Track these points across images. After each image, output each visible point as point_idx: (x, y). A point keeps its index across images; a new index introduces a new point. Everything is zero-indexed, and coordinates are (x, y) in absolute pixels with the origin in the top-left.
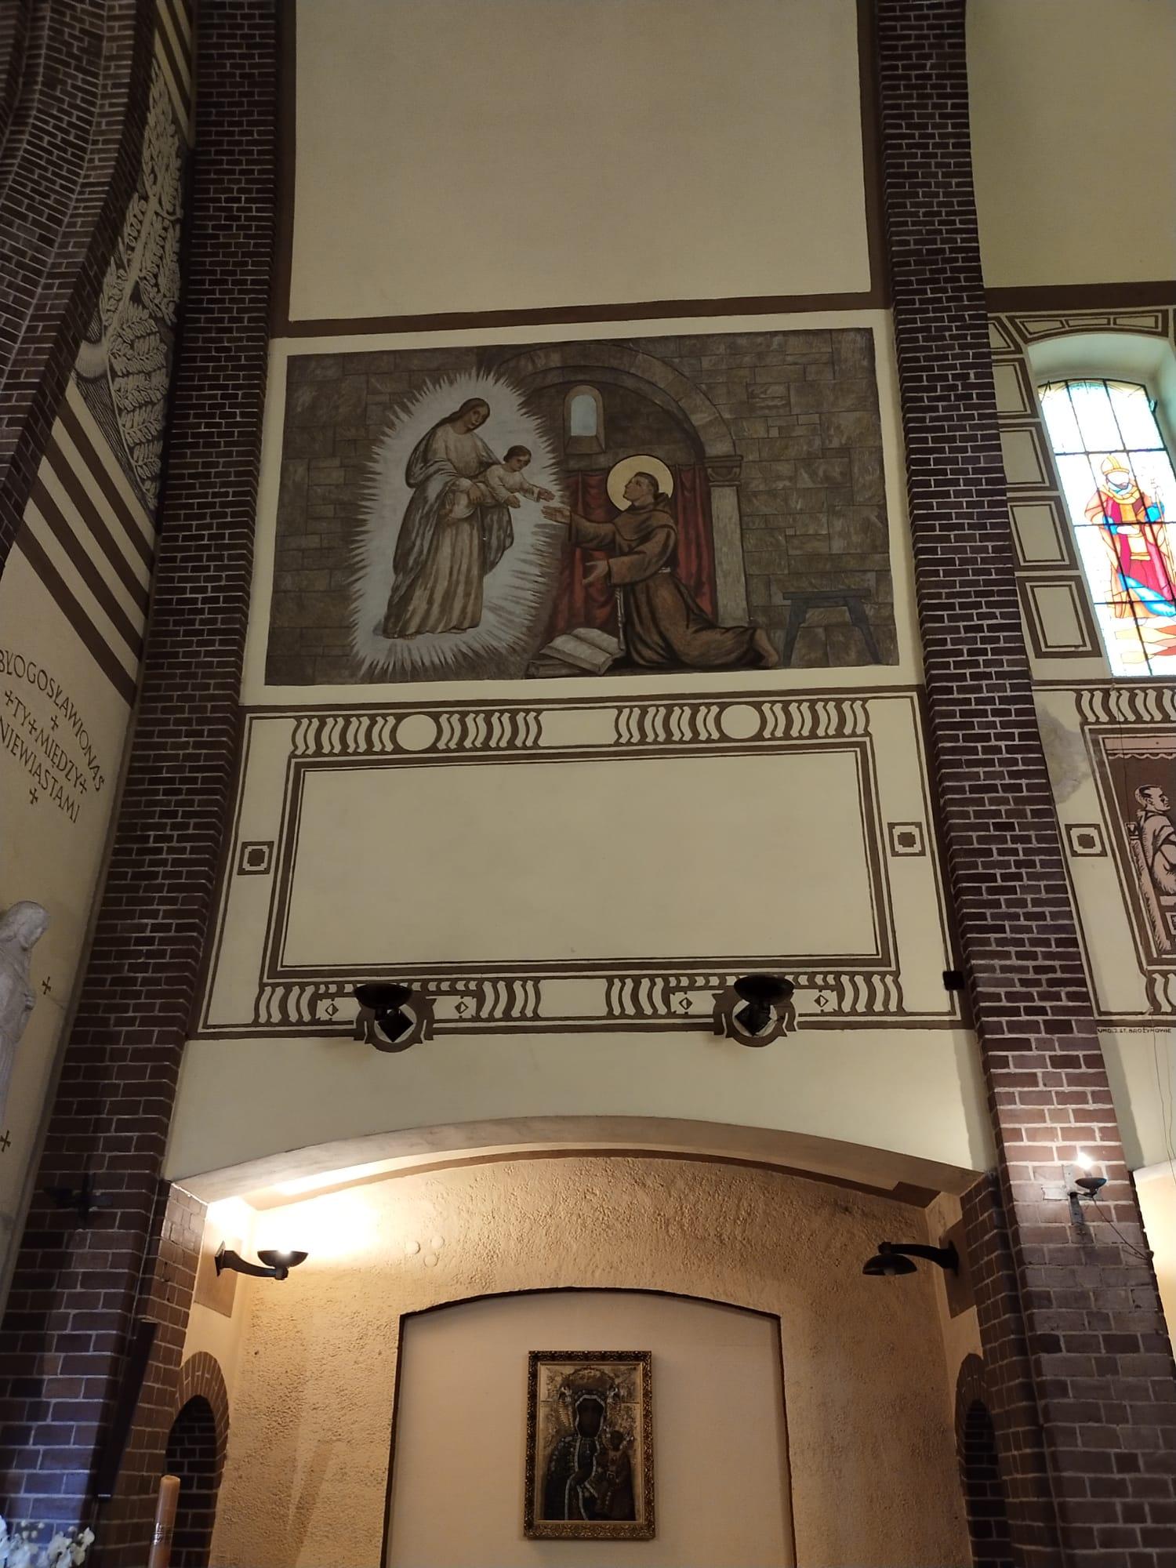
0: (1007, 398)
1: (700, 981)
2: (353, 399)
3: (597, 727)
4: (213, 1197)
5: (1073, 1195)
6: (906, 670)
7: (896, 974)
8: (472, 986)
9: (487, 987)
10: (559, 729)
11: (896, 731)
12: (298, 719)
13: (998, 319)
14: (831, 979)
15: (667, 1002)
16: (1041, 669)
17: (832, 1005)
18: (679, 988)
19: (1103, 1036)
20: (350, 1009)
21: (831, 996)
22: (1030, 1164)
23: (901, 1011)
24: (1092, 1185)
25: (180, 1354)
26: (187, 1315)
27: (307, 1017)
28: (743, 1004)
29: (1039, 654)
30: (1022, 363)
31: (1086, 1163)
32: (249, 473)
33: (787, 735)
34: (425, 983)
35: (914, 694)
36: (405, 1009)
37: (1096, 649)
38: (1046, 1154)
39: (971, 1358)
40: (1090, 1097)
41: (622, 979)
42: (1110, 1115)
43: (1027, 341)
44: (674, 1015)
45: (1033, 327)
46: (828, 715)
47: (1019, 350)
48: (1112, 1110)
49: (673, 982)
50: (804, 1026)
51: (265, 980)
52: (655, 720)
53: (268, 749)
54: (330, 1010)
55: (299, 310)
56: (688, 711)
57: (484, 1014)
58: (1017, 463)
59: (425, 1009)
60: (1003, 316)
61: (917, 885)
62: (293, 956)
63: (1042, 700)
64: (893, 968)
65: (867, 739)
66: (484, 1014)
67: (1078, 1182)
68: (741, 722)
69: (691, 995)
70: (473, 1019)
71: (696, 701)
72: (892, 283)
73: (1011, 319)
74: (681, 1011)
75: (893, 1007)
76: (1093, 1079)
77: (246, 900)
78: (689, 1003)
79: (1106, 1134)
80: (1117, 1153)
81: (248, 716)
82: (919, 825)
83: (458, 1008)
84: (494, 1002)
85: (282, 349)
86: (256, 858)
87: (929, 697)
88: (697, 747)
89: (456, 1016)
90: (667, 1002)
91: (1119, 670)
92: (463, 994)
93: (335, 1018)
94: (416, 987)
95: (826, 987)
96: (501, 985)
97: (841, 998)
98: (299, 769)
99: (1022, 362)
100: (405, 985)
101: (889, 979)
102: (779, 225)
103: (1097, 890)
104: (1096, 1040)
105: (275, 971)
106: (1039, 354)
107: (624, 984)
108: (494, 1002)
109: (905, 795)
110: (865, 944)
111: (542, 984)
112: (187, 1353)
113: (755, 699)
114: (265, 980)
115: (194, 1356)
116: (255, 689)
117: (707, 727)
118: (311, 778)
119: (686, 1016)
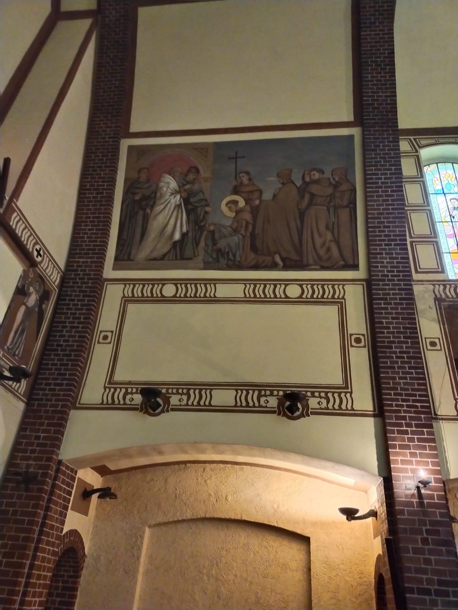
0: (408, 167)
1: (317, 394)
2: (151, 163)
3: (237, 291)
4: (103, 480)
5: (418, 488)
6: (361, 273)
7: (351, 393)
8: (185, 391)
9: (191, 392)
10: (223, 291)
11: (355, 298)
12: (125, 285)
13: (410, 139)
14: (323, 395)
15: (259, 401)
16: (415, 276)
17: (324, 405)
18: (265, 396)
19: (434, 424)
20: (138, 398)
21: (324, 401)
22: (401, 475)
23: (353, 409)
24: (425, 484)
25: (62, 529)
26: (66, 514)
27: (257, 404)
28: (288, 403)
29: (417, 272)
30: (418, 157)
31: (423, 474)
32: (112, 189)
33: (312, 297)
34: (168, 389)
35: (364, 283)
36: (159, 400)
37: (443, 272)
38: (406, 471)
39: (379, 555)
40: (416, 440)
41: (242, 390)
42: (436, 456)
43: (420, 147)
44: (262, 407)
45: (423, 142)
46: (329, 290)
47: (417, 151)
48: (437, 454)
49: (130, 390)
50: (313, 413)
51: (106, 385)
52: (269, 290)
53: (112, 296)
54: (266, 402)
55: (134, 128)
56: (272, 286)
57: (190, 403)
58: (412, 193)
59: (167, 401)
60: (412, 138)
61: (360, 358)
62: (118, 377)
63: (417, 289)
64: (350, 390)
65: (343, 301)
66: (190, 403)
67: (419, 482)
68: (294, 291)
69: (269, 398)
70: (185, 405)
71: (276, 282)
72: (360, 119)
73: (415, 139)
74: (264, 405)
75: (349, 408)
76: (432, 442)
77: (100, 354)
78: (268, 402)
79: (433, 464)
80: (439, 472)
81: (106, 283)
82: (363, 335)
83: (319, 403)
84: (194, 399)
85: (125, 144)
86: (106, 337)
87: (369, 284)
88: (275, 301)
89: (318, 407)
90: (259, 401)
91: (450, 278)
92: (181, 394)
93: (132, 403)
94: (164, 391)
95: (183, 394)
96: (336, 395)
97: (328, 402)
98: (126, 301)
99: (418, 156)
100: (160, 389)
101: (348, 395)
102: (321, 98)
103: (437, 364)
104: (432, 425)
105: (111, 383)
106: (425, 153)
107: (242, 392)
108: (194, 399)
109: (357, 324)
110: (337, 379)
111: (234, 404)
112: (66, 529)
113: (300, 282)
114: (106, 385)
115: (70, 531)
116: (109, 272)
117: (279, 291)
118: (131, 308)
119: (266, 407)
